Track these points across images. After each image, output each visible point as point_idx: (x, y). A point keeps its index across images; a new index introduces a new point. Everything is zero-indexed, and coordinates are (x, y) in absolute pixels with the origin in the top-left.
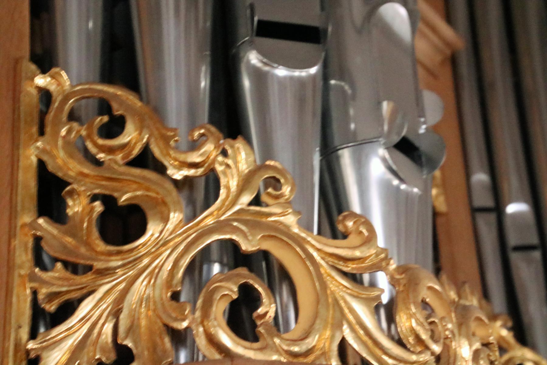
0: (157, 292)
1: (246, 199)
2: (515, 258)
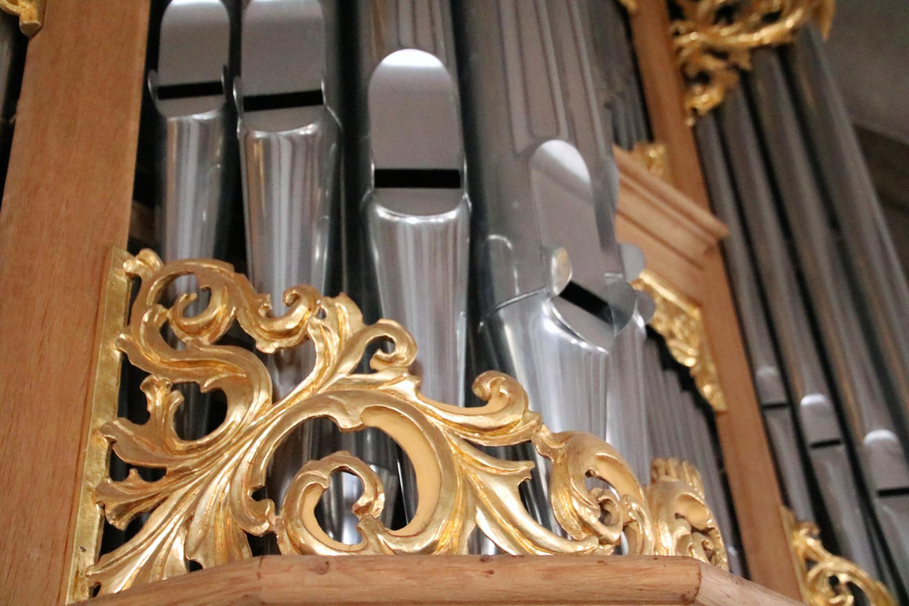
0: (235, 491)
1: (350, 364)
2: (816, 455)
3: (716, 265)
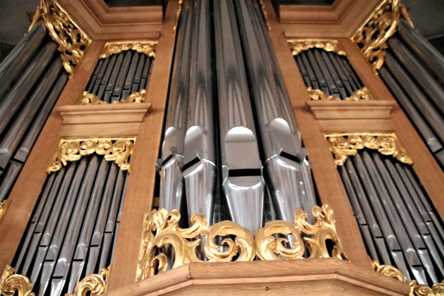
3: (400, 114)
